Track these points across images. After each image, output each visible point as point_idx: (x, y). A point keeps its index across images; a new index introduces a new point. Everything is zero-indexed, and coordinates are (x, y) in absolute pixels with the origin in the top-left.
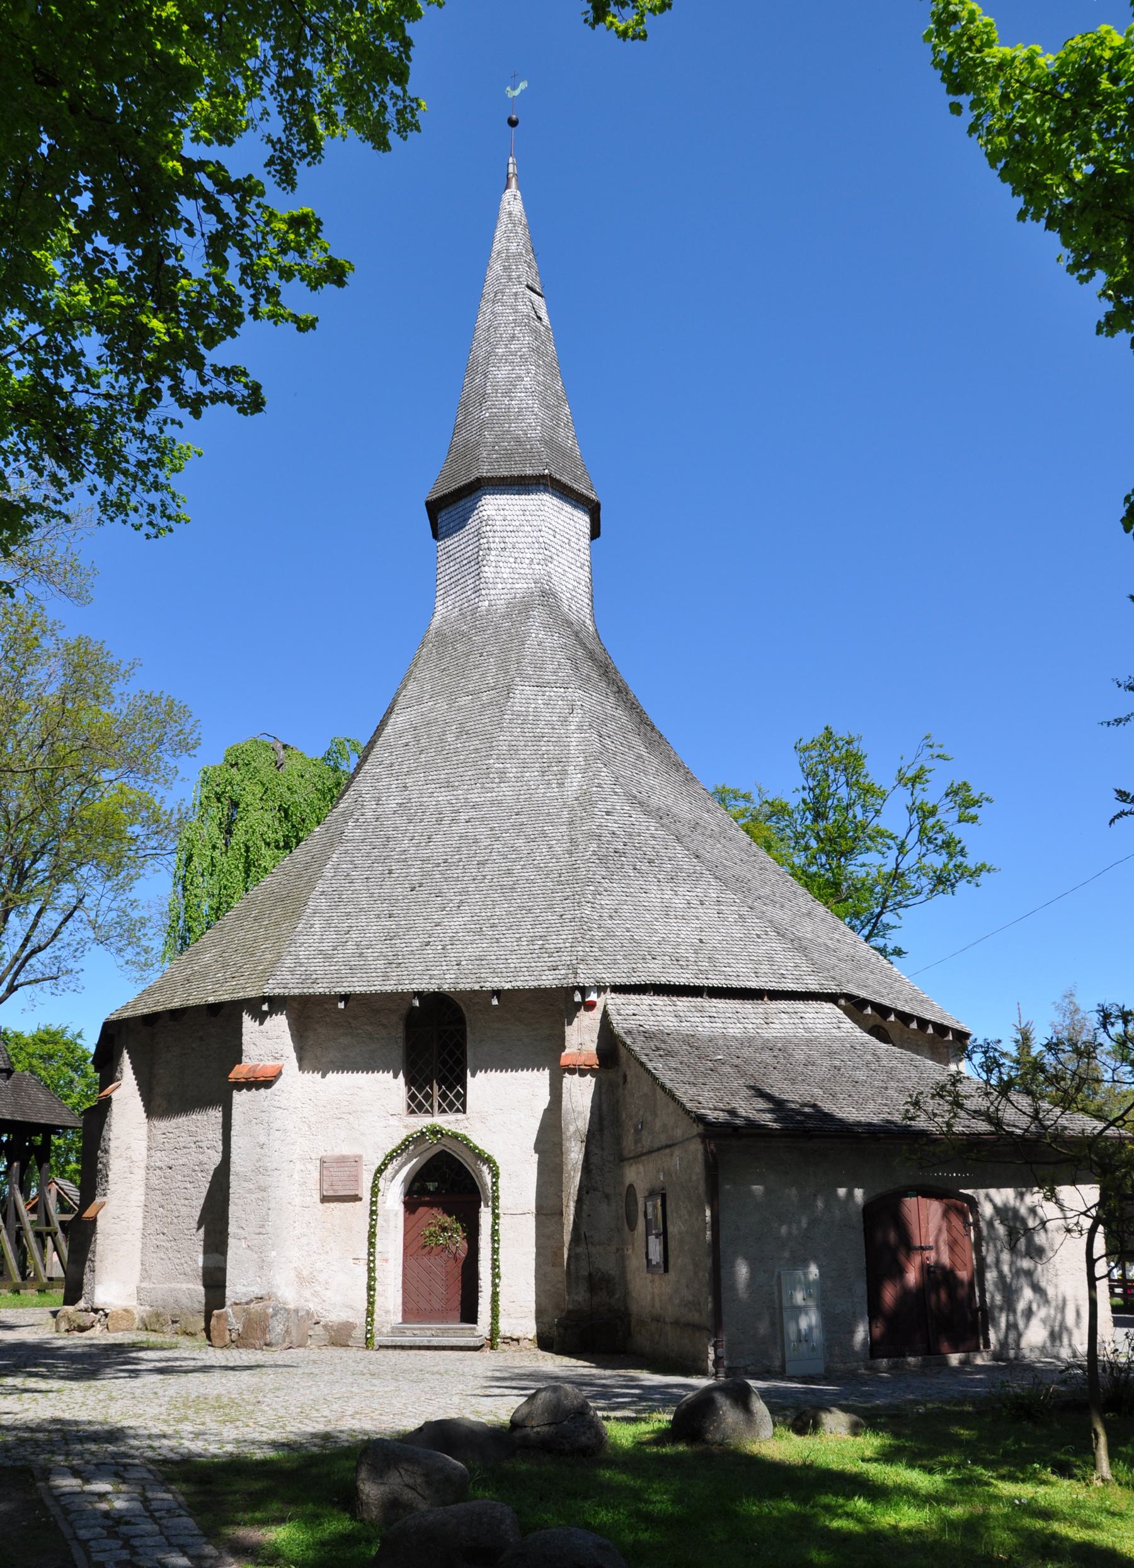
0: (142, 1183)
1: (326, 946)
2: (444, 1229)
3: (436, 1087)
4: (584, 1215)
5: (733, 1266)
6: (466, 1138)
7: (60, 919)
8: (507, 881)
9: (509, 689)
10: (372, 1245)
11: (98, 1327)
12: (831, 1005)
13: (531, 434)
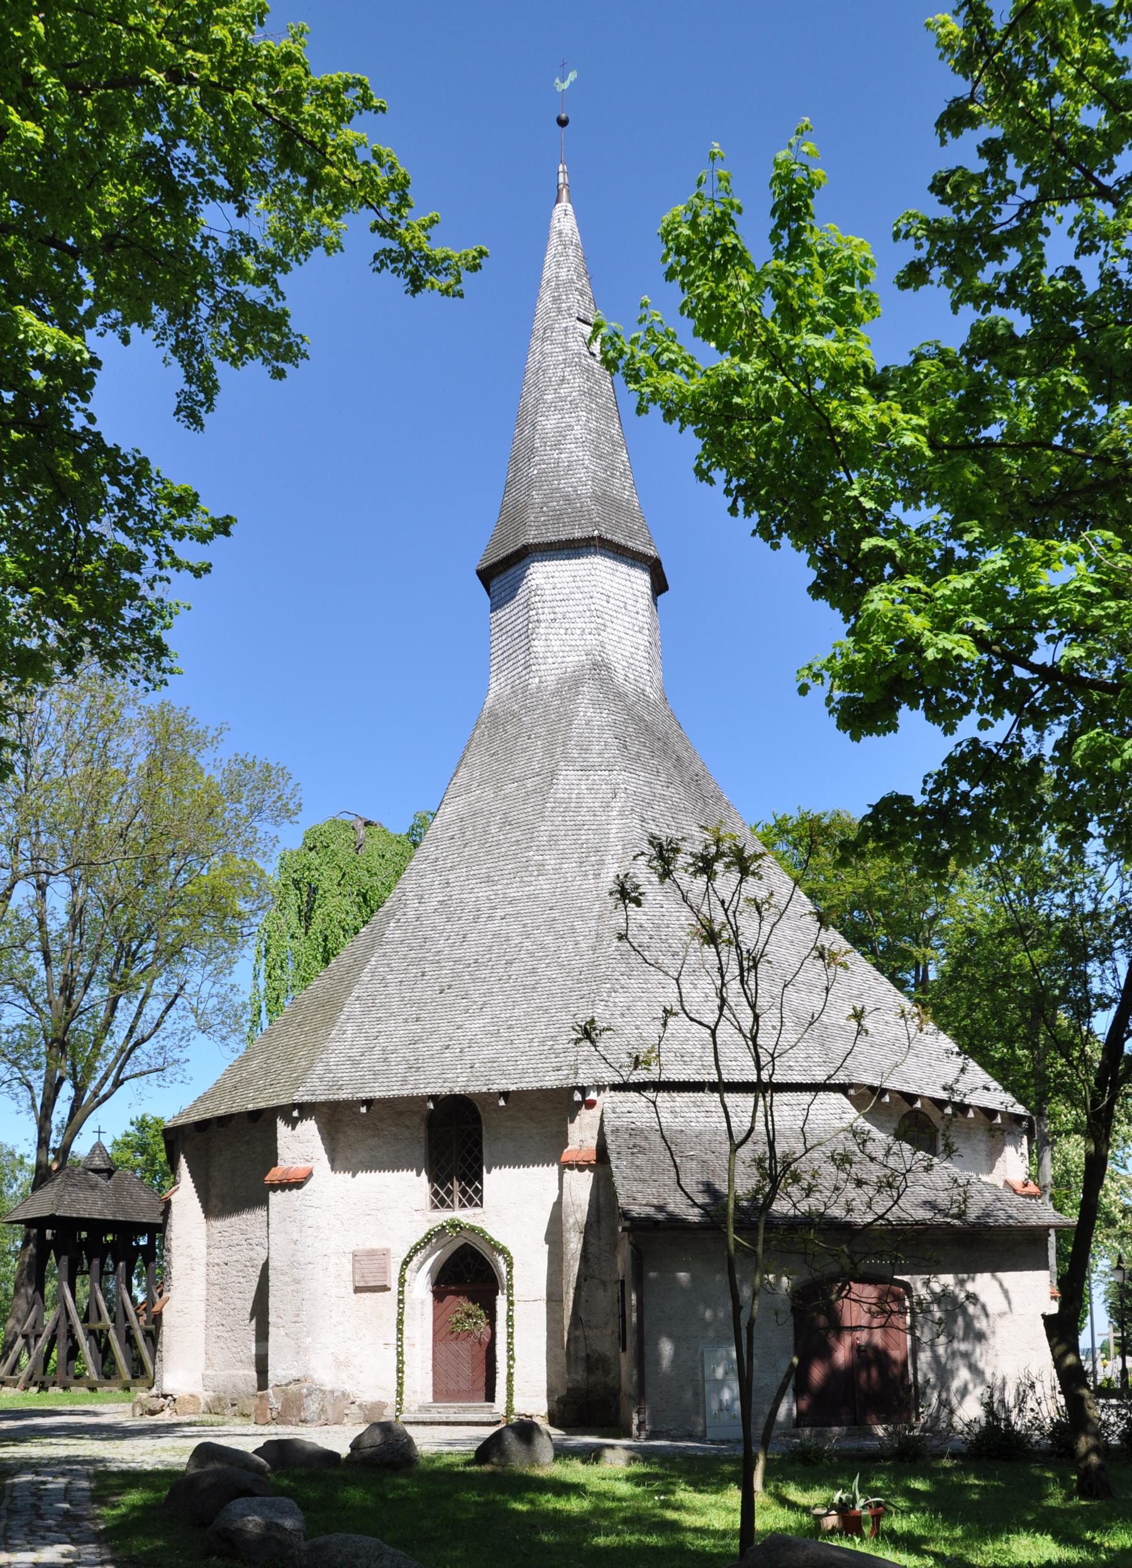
0: (203, 1279)
1: (354, 1053)
2: (469, 1316)
3: (456, 1183)
4: (583, 1300)
5: (657, 1344)
6: (482, 1231)
7: (163, 1007)
8: (530, 981)
9: (553, 774)
10: (400, 1331)
11: (168, 1411)
12: (840, 1096)
13: (582, 490)
